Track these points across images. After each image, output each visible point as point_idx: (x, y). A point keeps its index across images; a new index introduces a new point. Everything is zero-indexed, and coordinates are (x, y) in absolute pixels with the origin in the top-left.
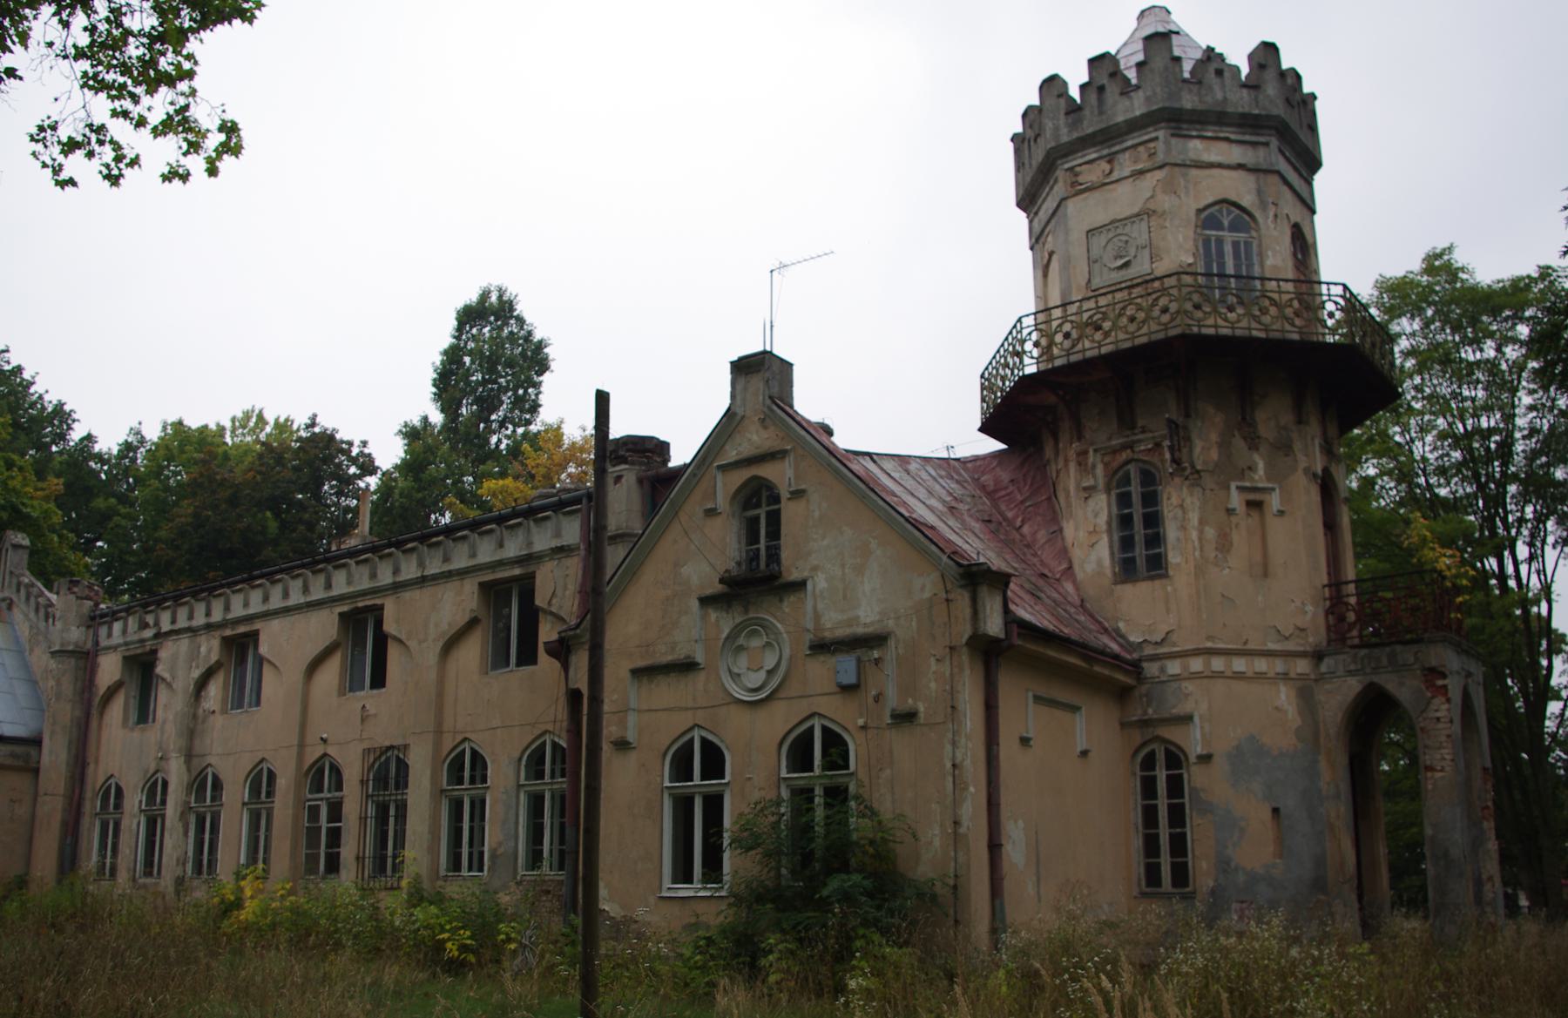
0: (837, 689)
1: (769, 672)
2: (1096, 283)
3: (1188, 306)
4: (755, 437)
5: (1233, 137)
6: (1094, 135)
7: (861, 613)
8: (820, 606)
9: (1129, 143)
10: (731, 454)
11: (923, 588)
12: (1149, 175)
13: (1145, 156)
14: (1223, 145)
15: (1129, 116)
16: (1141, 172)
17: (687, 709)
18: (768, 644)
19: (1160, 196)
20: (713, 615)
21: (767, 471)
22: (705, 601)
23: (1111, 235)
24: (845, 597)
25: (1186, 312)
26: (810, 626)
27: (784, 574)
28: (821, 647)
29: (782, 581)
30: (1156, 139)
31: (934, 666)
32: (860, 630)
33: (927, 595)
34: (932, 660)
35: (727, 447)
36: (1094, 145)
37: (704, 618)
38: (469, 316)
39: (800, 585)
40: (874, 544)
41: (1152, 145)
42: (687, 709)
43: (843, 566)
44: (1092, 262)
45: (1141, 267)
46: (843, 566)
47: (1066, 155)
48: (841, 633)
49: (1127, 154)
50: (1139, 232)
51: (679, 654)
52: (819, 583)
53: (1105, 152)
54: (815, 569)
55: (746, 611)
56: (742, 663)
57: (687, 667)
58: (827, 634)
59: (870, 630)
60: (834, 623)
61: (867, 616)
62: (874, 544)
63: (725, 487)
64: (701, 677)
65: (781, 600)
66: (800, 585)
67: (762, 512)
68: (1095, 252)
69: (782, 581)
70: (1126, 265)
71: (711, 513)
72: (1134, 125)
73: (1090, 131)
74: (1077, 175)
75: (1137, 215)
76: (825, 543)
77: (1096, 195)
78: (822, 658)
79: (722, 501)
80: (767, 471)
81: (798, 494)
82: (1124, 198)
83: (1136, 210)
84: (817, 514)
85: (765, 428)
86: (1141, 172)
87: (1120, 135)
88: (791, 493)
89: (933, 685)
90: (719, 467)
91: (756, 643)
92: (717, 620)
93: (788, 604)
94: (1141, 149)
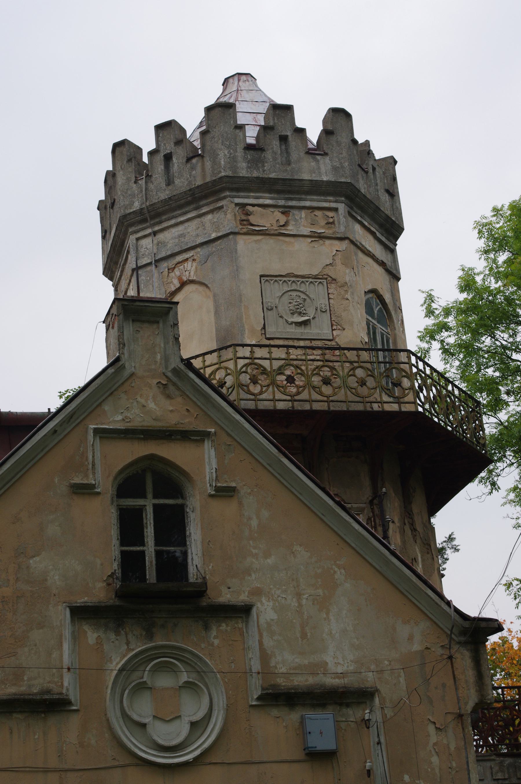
0: (300, 755)
1: (193, 725)
2: (271, 331)
3: (316, 380)
4: (152, 405)
5: (378, 234)
6: (276, 181)
7: (329, 659)
8: (268, 643)
9: (308, 204)
10: (114, 418)
11: (411, 638)
12: (328, 242)
13: (323, 223)
14: (370, 237)
15: (315, 177)
16: (321, 237)
17: (46, 771)
18: (189, 685)
19: (340, 267)
20: (92, 635)
21: (174, 453)
22: (81, 613)
23: (286, 289)
24: (304, 635)
25: (241, 386)
26: (256, 666)
27: (210, 592)
28: (279, 697)
29: (204, 602)
30: (336, 210)
31: (434, 738)
32: (330, 681)
33: (416, 647)
34: (431, 729)
35: (106, 407)
36: (270, 191)
37: (76, 638)
38: (367, 140)
39: (244, 611)
40: (339, 575)
41: (330, 214)
42: (46, 771)
43: (299, 595)
44: (267, 309)
45: (321, 329)
46: (299, 595)
47: (238, 190)
48: (302, 681)
49: (303, 213)
50: (318, 293)
51: (34, 684)
52: (265, 611)
53: (281, 202)
54: (257, 592)
55: (150, 636)
56: (143, 709)
57: (50, 706)
58: (280, 681)
59: (337, 682)
60: (289, 666)
61: (338, 661)
62: (339, 575)
63: (107, 463)
64: (74, 722)
65: (207, 628)
66: (244, 611)
67: (148, 504)
68: (269, 300)
69: (204, 602)
70: (305, 323)
71: (84, 490)
72: (317, 188)
73: (273, 175)
74: (248, 214)
75: (316, 277)
76: (270, 561)
77: (271, 241)
78: (275, 712)
79: (104, 480)
80: (174, 453)
81: (224, 493)
82: (302, 256)
83: (315, 272)
84: (254, 523)
85: (169, 397)
86: (321, 237)
87: (298, 192)
88: (218, 489)
89: (435, 760)
90: (96, 431)
91: (164, 681)
92: (99, 642)
93: (218, 634)
94: (318, 213)
